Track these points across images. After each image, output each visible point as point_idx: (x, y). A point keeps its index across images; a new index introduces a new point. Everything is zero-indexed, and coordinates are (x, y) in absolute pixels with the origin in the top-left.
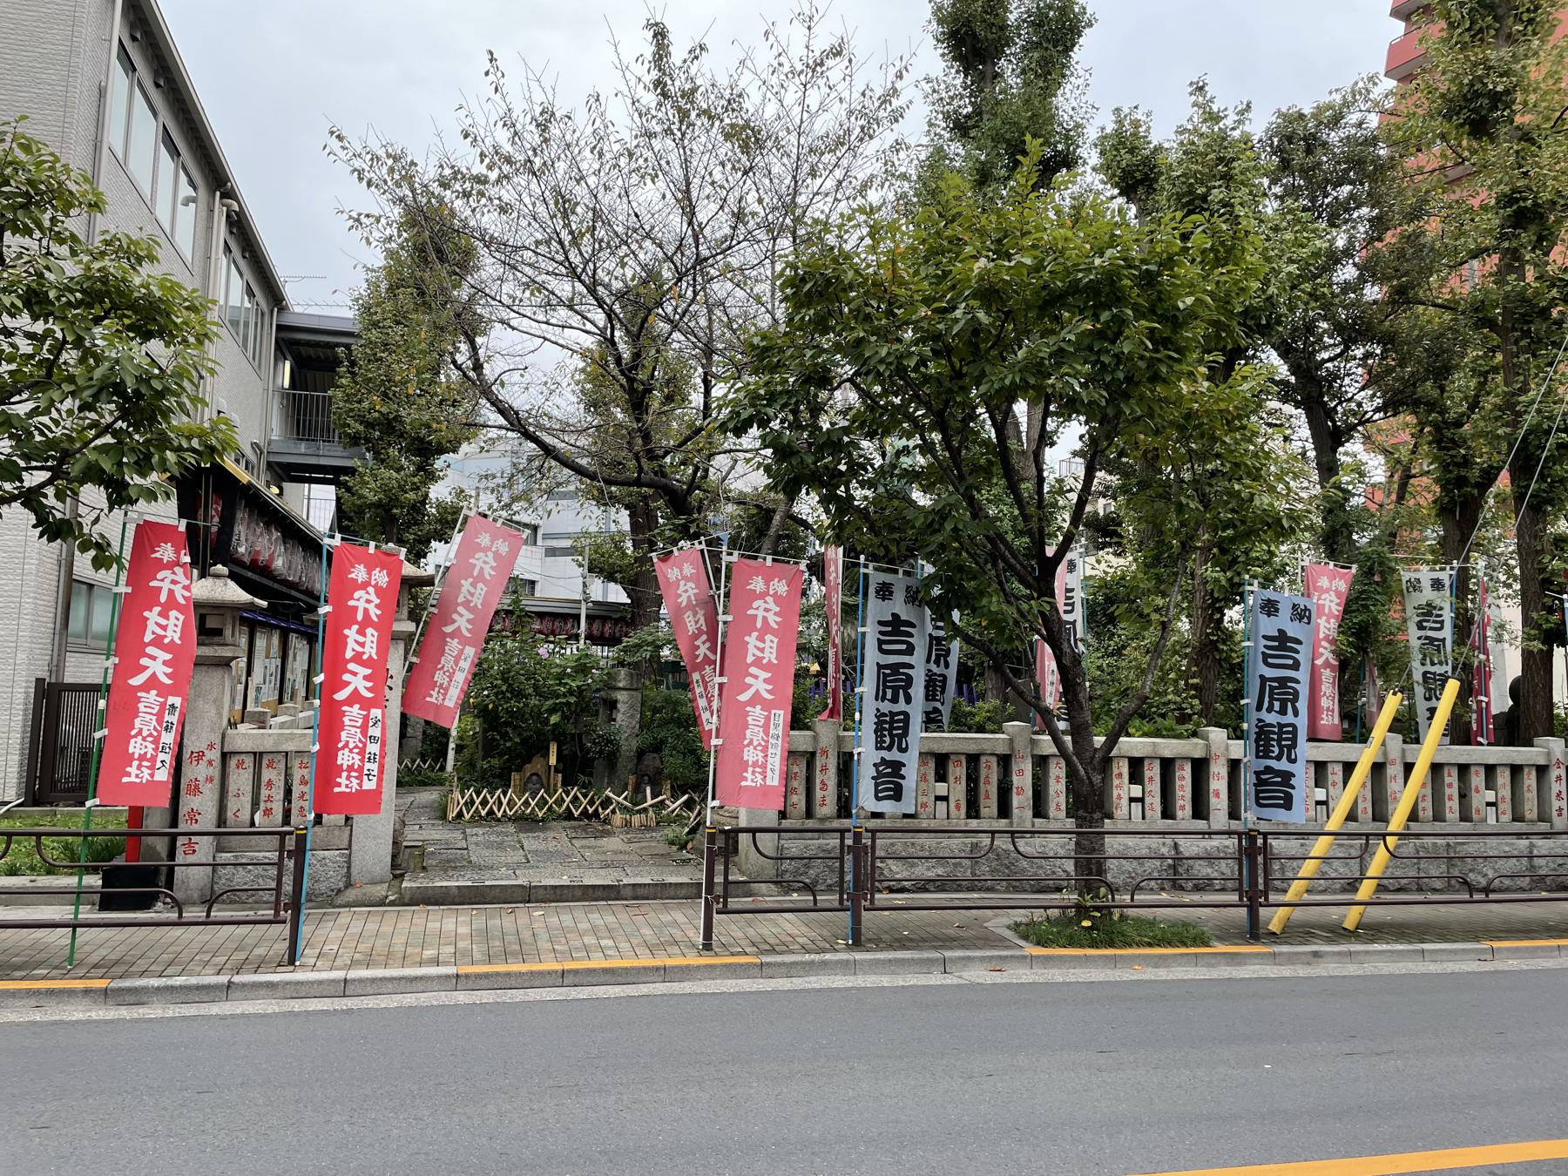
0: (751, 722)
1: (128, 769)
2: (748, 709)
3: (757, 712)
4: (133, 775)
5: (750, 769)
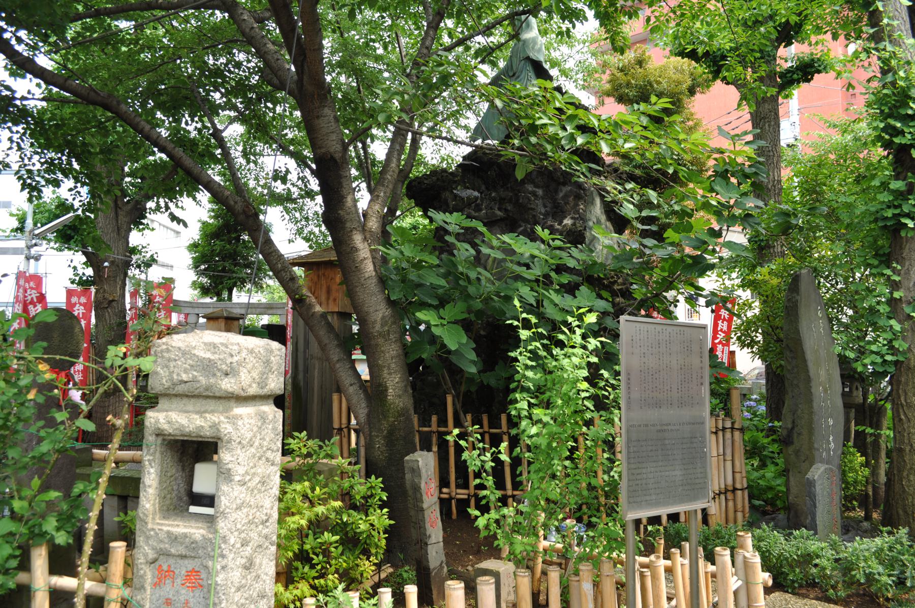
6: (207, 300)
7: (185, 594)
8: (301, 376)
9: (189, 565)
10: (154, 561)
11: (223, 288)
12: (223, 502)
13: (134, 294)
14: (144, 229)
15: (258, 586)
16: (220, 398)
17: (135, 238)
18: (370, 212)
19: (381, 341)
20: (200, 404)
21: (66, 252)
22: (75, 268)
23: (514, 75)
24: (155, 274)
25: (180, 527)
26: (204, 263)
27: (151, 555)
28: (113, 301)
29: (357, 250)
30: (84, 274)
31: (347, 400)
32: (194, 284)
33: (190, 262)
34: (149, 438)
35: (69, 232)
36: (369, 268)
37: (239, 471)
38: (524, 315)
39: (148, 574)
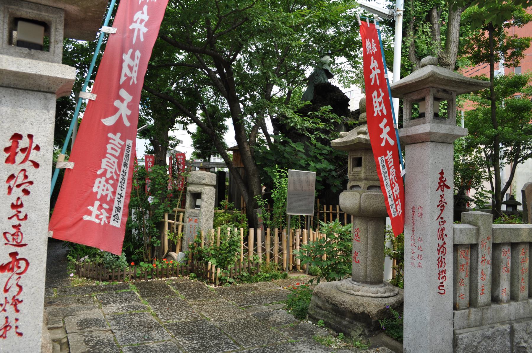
0: (109, 150)
1: (90, 208)
2: (110, 135)
3: (116, 139)
4: (94, 215)
5: (97, 203)
6: (199, 161)
7: (194, 224)
8: (232, 190)
9: (195, 218)
10: (189, 217)
11: (206, 155)
12: (202, 206)
13: (171, 158)
14: (174, 130)
15: (209, 225)
16: (202, 184)
17: (170, 133)
18: (251, 135)
19: (252, 177)
20: (198, 186)
21: (142, 139)
22: (147, 146)
23: (317, 75)
24: (178, 148)
25: (193, 211)
26: (198, 144)
27: (188, 216)
28: (162, 160)
29: (245, 148)
30: (150, 149)
31: (243, 197)
32: (194, 153)
33: (192, 143)
34: (188, 192)
35: (145, 132)
36: (249, 153)
37: (205, 199)
38: (278, 169)
39: (187, 220)
